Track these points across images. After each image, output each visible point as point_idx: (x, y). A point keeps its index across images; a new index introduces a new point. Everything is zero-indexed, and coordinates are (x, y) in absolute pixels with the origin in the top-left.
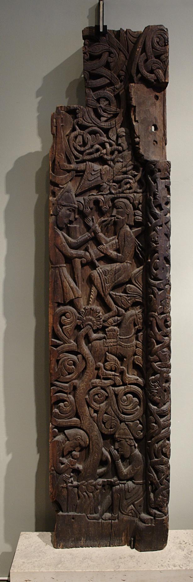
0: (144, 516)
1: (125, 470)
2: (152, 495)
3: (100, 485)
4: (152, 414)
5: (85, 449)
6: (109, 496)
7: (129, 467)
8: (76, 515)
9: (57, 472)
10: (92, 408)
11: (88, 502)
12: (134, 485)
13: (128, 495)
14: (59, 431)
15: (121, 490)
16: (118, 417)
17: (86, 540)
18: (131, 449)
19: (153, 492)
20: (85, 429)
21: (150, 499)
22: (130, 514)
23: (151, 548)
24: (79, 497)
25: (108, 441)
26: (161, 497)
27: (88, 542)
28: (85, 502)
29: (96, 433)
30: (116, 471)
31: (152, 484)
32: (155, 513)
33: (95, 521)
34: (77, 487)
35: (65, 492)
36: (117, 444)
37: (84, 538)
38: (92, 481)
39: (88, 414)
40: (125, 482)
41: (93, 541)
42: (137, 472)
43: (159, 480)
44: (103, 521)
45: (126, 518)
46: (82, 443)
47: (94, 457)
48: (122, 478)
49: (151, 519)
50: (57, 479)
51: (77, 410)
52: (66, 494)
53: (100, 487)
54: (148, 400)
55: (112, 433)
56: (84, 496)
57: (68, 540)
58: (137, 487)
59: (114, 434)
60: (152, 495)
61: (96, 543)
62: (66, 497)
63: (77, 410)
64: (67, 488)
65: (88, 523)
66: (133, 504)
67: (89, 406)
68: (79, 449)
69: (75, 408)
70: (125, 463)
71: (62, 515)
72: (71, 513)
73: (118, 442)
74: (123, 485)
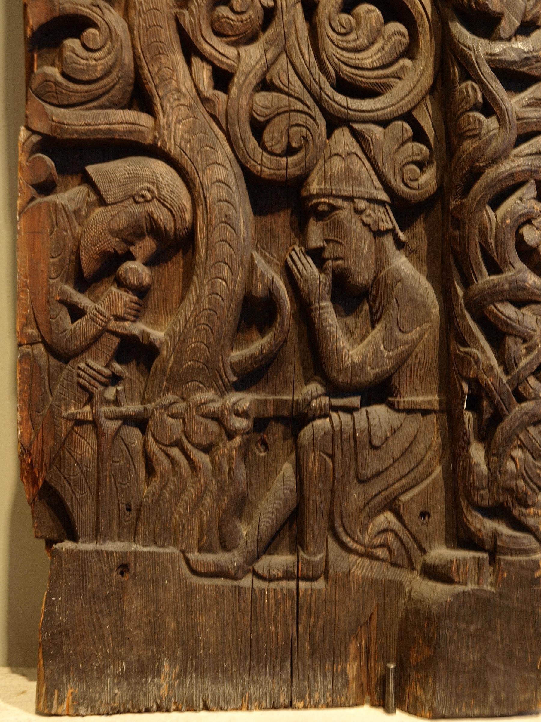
0: (441, 553)
1: (354, 348)
2: (477, 453)
3: (245, 414)
4: (469, 72)
5: (176, 246)
6: (287, 468)
7: (376, 334)
8: (135, 553)
9: (51, 349)
10: (204, 58)
11: (192, 491)
12: (396, 418)
13: (371, 463)
14: (62, 170)
15: (336, 434)
16: (318, 101)
17: (184, 673)
18: (380, 249)
19: (485, 434)
20: (174, 151)
21: (469, 467)
22: (381, 553)
23: (481, 702)
24: (150, 470)
25: (281, 221)
26: (518, 453)
27: (193, 686)
28: (177, 495)
29: (221, 173)
30: (317, 359)
31: (478, 394)
32: (496, 535)
33: (220, 582)
34: (140, 422)
35: (86, 446)
36: (316, 235)
37: (173, 659)
38: (209, 394)
39: (187, 86)
40: (356, 401)
41: (215, 680)
42: (408, 355)
43: (507, 372)
44: (259, 584)
45: (360, 568)
46: (162, 215)
47: (218, 285)
48: (344, 379)
49: (479, 563)
50: (52, 379)
51: (137, 68)
52: (90, 455)
53: (240, 423)
54: (448, 12)
55: (293, 171)
56: (173, 462)
57: (101, 670)
58: (411, 425)
59: (302, 179)
60: (477, 453)
61: (227, 689)
62: (91, 467)
63: (137, 68)
64: (95, 424)
65: (190, 592)
66: (392, 505)
67: (190, 50)
68: (147, 246)
69: (128, 57)
70: (349, 320)
71: (70, 552)
72: (110, 546)
73: (321, 216)
74: (346, 417)
